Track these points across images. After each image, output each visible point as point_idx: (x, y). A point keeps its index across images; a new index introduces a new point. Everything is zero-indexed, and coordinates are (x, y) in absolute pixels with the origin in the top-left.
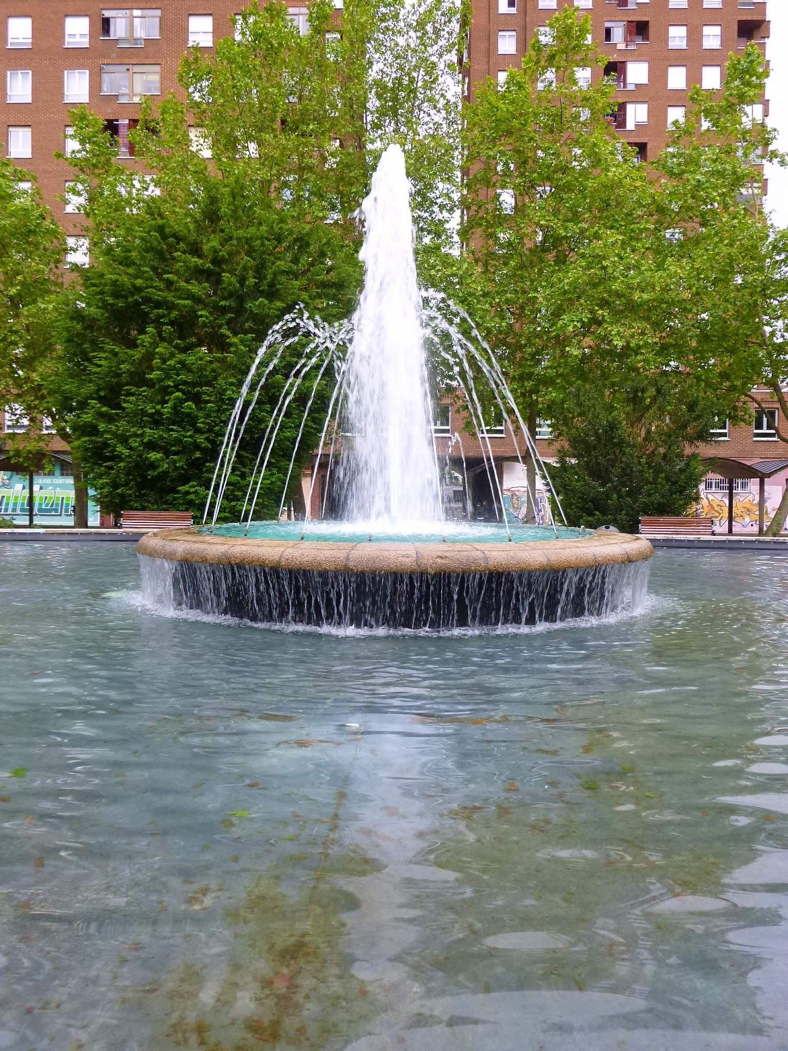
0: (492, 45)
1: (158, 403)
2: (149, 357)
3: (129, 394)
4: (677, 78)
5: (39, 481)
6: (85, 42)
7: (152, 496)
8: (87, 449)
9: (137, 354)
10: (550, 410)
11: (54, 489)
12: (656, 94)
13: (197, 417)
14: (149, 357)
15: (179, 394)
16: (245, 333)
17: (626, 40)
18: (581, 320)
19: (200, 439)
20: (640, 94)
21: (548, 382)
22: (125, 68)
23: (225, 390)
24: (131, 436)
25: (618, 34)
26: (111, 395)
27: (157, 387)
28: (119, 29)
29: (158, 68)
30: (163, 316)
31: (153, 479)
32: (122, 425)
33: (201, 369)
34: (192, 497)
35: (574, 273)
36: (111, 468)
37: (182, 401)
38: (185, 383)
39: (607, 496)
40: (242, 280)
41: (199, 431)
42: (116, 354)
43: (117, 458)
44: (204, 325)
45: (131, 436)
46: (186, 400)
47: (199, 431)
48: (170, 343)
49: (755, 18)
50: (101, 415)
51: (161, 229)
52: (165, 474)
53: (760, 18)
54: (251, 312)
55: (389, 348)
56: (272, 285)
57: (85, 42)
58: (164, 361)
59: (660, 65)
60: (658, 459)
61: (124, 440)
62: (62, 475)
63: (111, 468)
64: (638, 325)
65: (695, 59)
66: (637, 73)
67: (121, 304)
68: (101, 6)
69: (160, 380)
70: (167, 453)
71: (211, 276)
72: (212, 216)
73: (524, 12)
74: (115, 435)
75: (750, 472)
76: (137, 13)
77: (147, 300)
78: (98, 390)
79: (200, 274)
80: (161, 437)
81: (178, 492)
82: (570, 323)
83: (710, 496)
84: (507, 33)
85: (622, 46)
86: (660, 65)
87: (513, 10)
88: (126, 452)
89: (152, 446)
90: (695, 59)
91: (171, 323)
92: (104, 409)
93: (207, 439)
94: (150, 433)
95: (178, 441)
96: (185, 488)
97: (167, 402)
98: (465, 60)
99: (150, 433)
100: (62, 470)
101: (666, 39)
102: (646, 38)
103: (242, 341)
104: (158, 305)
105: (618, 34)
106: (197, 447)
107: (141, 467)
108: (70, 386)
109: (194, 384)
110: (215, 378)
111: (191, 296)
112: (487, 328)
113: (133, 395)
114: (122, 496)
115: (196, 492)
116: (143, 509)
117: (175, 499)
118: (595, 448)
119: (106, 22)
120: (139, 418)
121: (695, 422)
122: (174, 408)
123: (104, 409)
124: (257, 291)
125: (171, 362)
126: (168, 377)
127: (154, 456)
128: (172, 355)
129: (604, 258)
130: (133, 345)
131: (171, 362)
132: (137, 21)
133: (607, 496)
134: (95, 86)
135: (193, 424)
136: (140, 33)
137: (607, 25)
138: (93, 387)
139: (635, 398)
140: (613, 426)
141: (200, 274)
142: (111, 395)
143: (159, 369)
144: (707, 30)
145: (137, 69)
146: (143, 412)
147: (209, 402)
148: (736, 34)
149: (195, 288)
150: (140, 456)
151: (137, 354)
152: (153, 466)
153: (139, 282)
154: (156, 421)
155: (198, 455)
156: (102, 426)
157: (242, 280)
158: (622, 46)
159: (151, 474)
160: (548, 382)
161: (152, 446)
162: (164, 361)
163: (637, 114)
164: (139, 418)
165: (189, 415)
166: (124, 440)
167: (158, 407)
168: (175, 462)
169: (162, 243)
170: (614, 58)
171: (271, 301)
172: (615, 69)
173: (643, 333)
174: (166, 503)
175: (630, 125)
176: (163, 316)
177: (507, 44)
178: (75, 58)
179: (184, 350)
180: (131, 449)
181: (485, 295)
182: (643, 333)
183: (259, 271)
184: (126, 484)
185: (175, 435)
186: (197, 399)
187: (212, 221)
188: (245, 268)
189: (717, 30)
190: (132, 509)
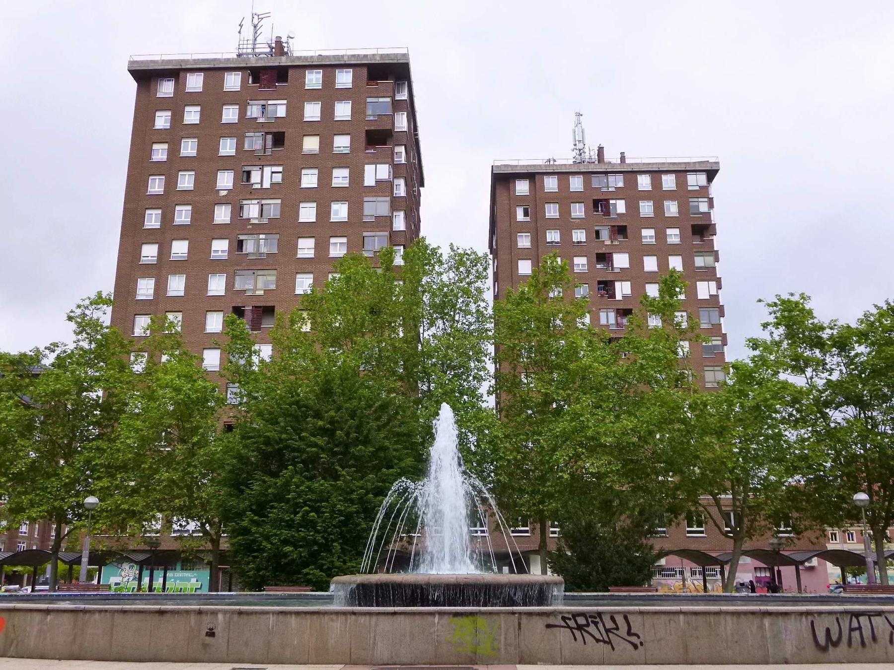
0: (513, 242)
1: (291, 513)
2: (287, 484)
3: (272, 507)
4: (650, 264)
5: (169, 574)
6: (225, 256)
7: (283, 576)
8: (240, 545)
9: (279, 482)
10: (555, 515)
11: (175, 581)
12: (635, 274)
13: (317, 522)
14: (287, 484)
15: (306, 508)
16: (350, 467)
17: (610, 238)
18: (568, 455)
19: (319, 538)
20: (624, 275)
21: (550, 496)
22: (252, 272)
23: (336, 505)
24: (272, 536)
25: (605, 235)
26: (261, 508)
27: (291, 503)
28: (249, 247)
29: (275, 272)
30: (297, 457)
31: (286, 564)
32: (268, 528)
33: (321, 492)
34: (310, 577)
35: (562, 425)
36: (257, 557)
37: (307, 512)
38: (310, 500)
39: (590, 574)
40: (348, 434)
41: (318, 532)
42: (264, 482)
43: (263, 550)
44: (324, 463)
45: (272, 536)
46: (310, 512)
47: (318, 532)
48: (301, 474)
49: (704, 223)
50: (253, 522)
51: (297, 403)
52: (293, 560)
53: (707, 223)
54: (354, 454)
55: (445, 492)
56: (367, 437)
57: (225, 256)
58: (298, 487)
59: (638, 253)
60: (622, 548)
61: (267, 538)
62: (182, 569)
63: (257, 557)
64: (606, 458)
65: (662, 250)
66: (621, 261)
67: (270, 449)
68: (238, 232)
69: (294, 499)
70: (296, 547)
71: (329, 433)
72: (327, 392)
73: (535, 220)
74: (262, 535)
75: (714, 561)
76: (262, 236)
77: (287, 447)
78: (252, 505)
79: (323, 431)
80: (293, 536)
81: (300, 573)
82: (561, 456)
83: (695, 582)
84: (524, 234)
85: (608, 242)
86: (638, 253)
87: (528, 219)
88: (269, 546)
89: (286, 542)
90: (662, 250)
91: (303, 462)
92: (256, 518)
93: (322, 537)
94: (286, 533)
95: (304, 538)
96: (304, 571)
97: (298, 513)
98: (494, 247)
99: (286, 533)
100: (182, 566)
101: (640, 237)
102: (626, 237)
103: (348, 473)
104: (294, 450)
105: (605, 235)
106: (315, 542)
107: (277, 556)
108: (233, 502)
109: (316, 501)
110: (329, 497)
111: (316, 445)
112: (507, 460)
113: (275, 508)
114: (263, 577)
115: (313, 574)
116: (276, 585)
117: (298, 579)
118: (580, 541)
119: (240, 243)
120: (279, 523)
121: (646, 522)
122: (303, 517)
123: (256, 518)
124: (357, 442)
125: (302, 488)
126: (300, 496)
127: (288, 549)
128: (303, 482)
129: (582, 415)
130: (275, 475)
131: (302, 488)
132: (262, 242)
133: (590, 574)
134: (229, 285)
135: (314, 527)
136: (264, 250)
137: (596, 228)
138: (247, 503)
139: (606, 506)
140: (590, 526)
141: (323, 431)
142: (261, 508)
143: (295, 491)
144: (669, 231)
145: (260, 272)
146: (282, 520)
147: (324, 513)
148: (691, 233)
149: (321, 441)
150: (278, 549)
151: (279, 482)
152: (286, 555)
153: (284, 436)
154: (290, 525)
155: (316, 548)
156: (254, 529)
157: (348, 434)
158: (608, 242)
159: (284, 561)
160: (550, 496)
161: (286, 542)
162: (298, 487)
163: (623, 289)
164: (279, 523)
165: (312, 521)
166: (267, 538)
167: (292, 516)
168: (300, 552)
169: (297, 413)
170: (603, 250)
171: (366, 447)
172: (604, 258)
173: (610, 464)
174: (292, 582)
175: (619, 297)
176: (297, 457)
177: (524, 242)
178: (218, 266)
179: (310, 479)
180: (272, 543)
181: (506, 437)
182: (610, 464)
183: (359, 429)
184: (266, 569)
185: (302, 534)
186: (317, 510)
187: (326, 394)
188: (350, 427)
189: (676, 231)
190: (268, 585)
